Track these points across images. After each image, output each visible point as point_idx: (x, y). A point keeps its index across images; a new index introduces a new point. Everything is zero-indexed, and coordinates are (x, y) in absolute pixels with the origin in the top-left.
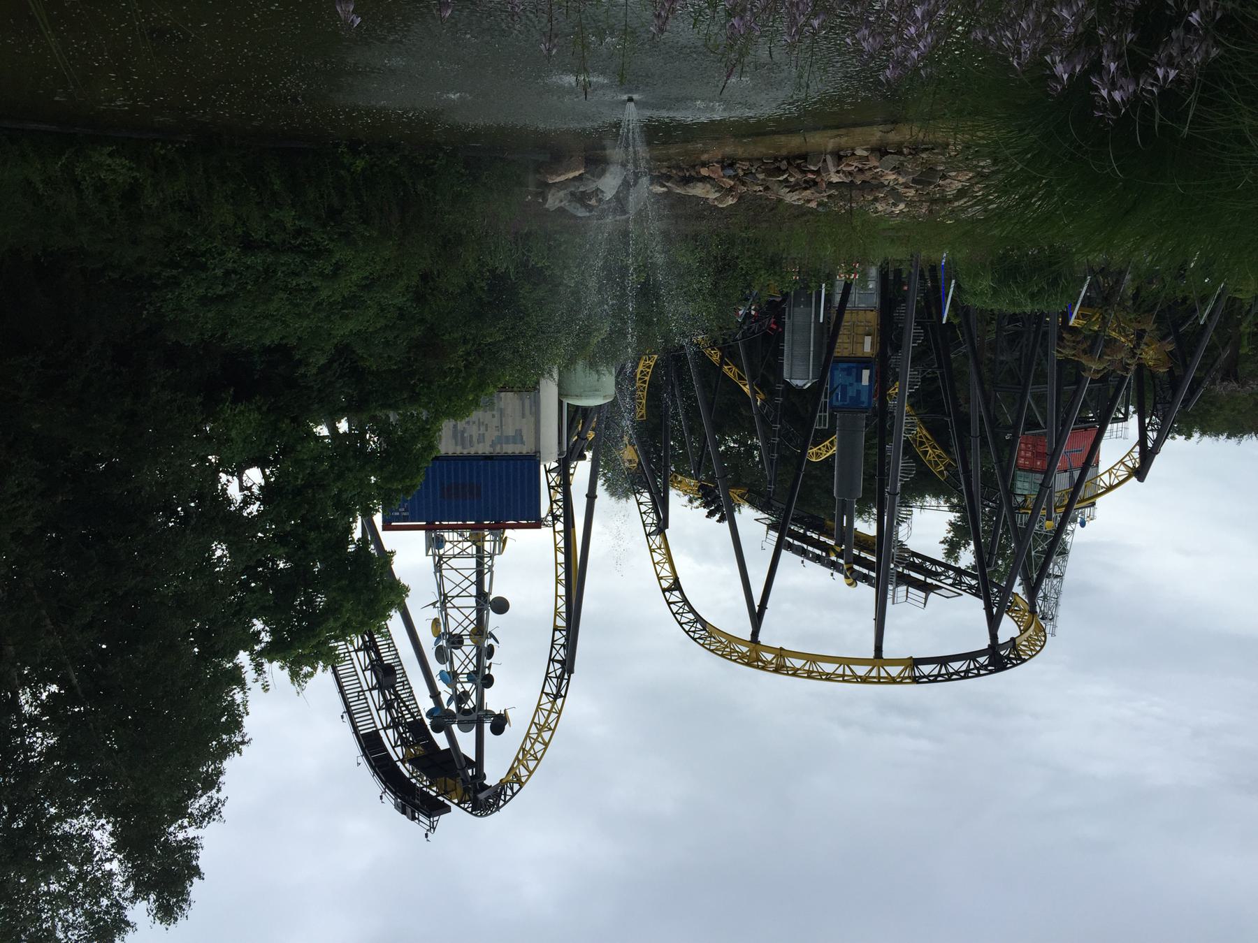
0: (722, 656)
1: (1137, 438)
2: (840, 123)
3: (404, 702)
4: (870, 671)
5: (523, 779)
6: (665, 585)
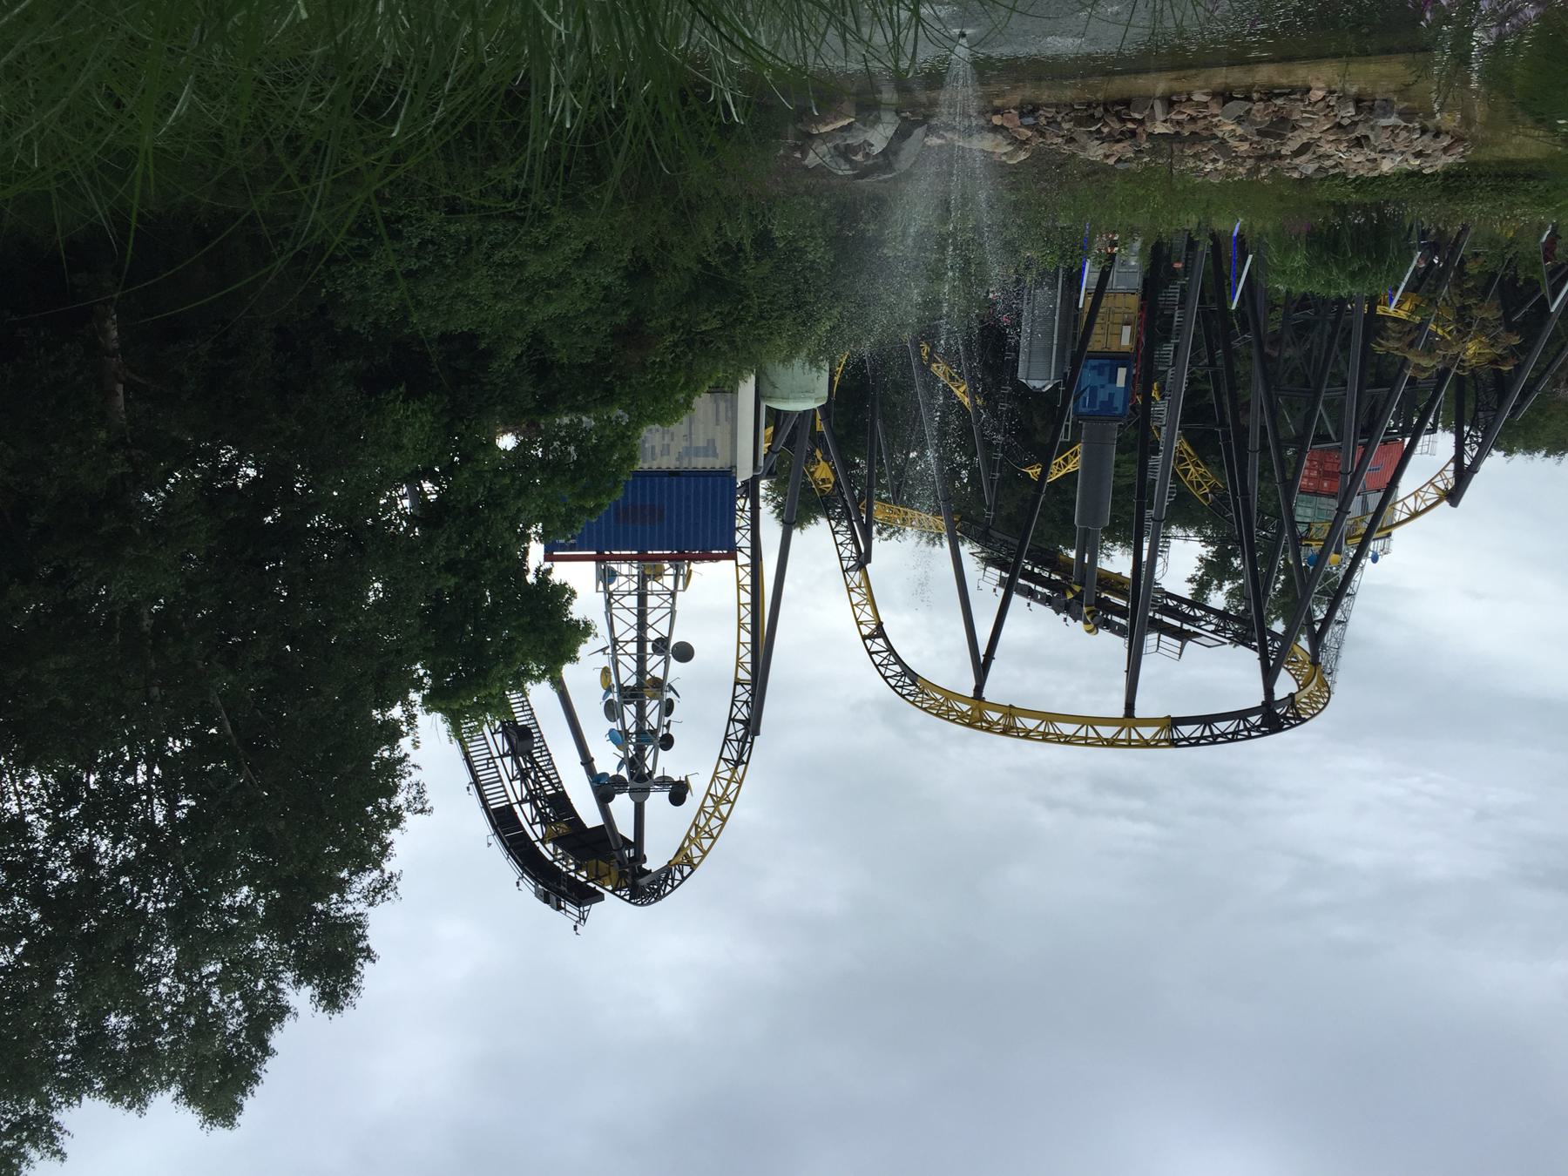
0: (937, 715)
3: (543, 771)
4: (1120, 732)
5: (696, 861)
6: (866, 631)
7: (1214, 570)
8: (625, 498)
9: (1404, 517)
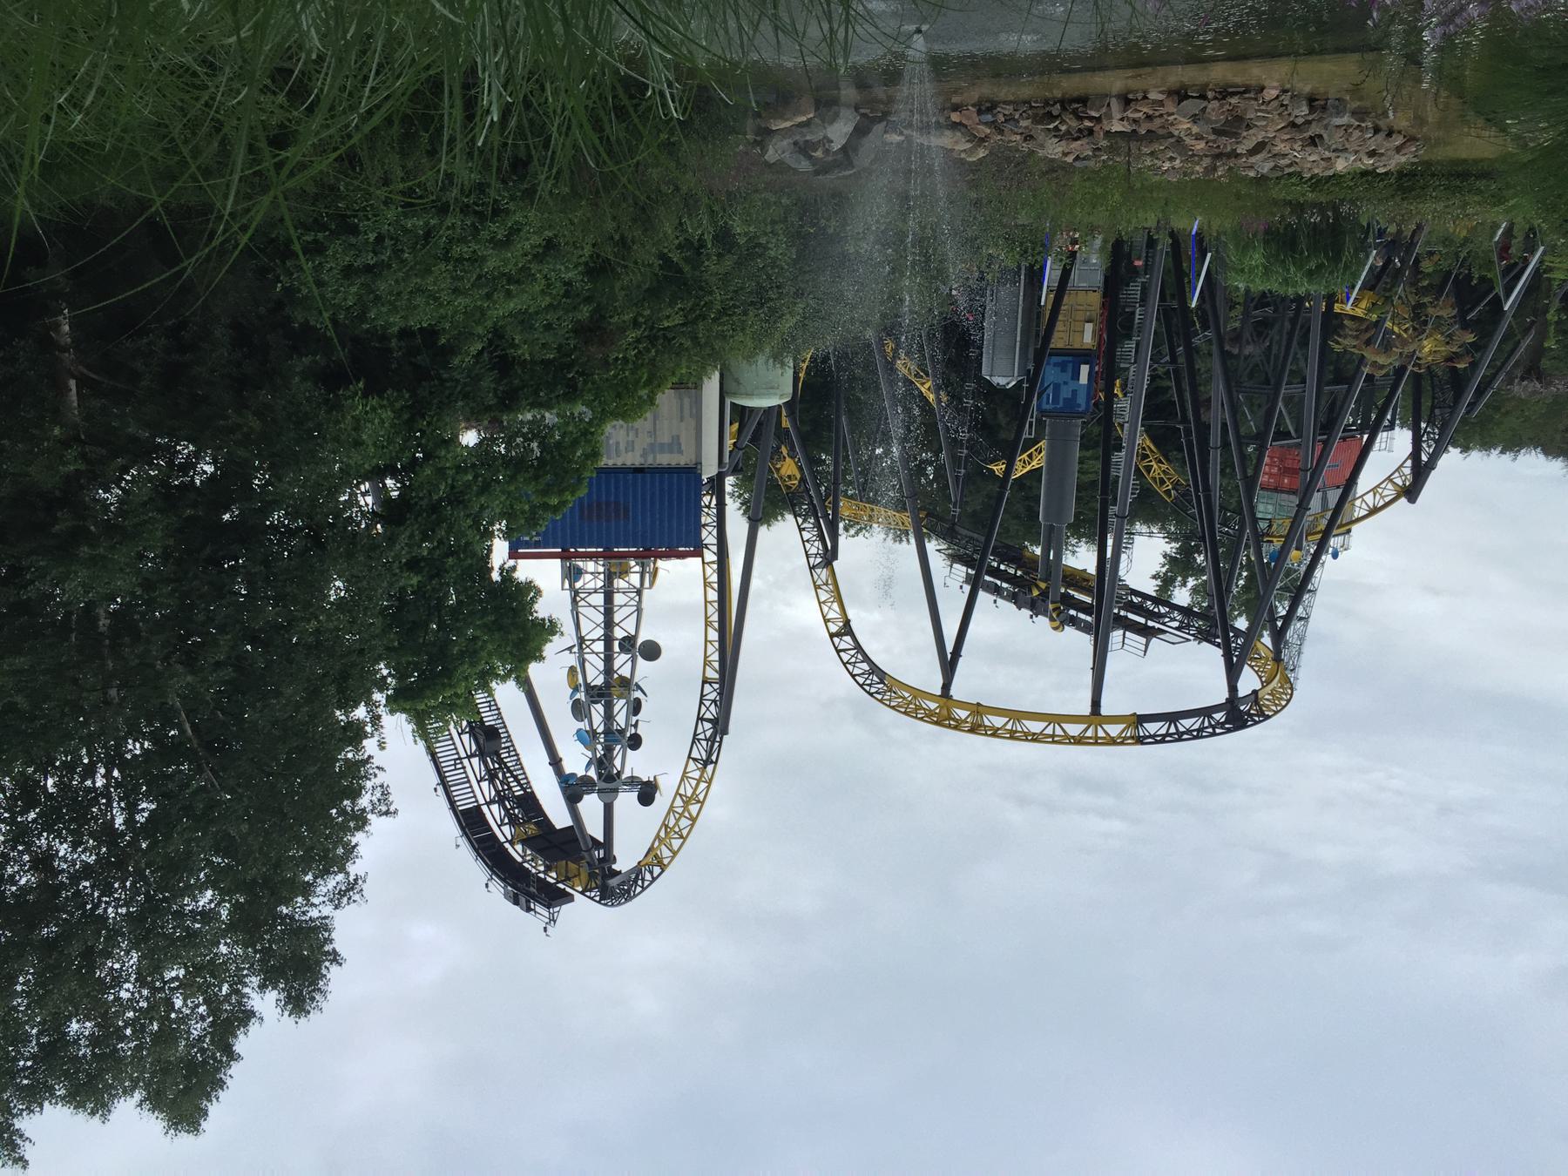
0: (905, 713)
1: (1409, 449)
2: (1137, 60)
3: (511, 772)
4: (1086, 730)
5: (666, 861)
6: (834, 628)
7: (1178, 567)
8: (589, 494)
9: (1363, 513)
